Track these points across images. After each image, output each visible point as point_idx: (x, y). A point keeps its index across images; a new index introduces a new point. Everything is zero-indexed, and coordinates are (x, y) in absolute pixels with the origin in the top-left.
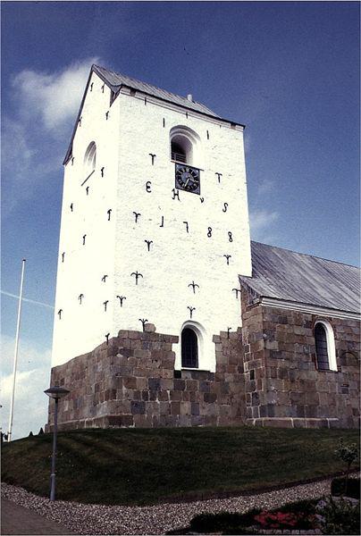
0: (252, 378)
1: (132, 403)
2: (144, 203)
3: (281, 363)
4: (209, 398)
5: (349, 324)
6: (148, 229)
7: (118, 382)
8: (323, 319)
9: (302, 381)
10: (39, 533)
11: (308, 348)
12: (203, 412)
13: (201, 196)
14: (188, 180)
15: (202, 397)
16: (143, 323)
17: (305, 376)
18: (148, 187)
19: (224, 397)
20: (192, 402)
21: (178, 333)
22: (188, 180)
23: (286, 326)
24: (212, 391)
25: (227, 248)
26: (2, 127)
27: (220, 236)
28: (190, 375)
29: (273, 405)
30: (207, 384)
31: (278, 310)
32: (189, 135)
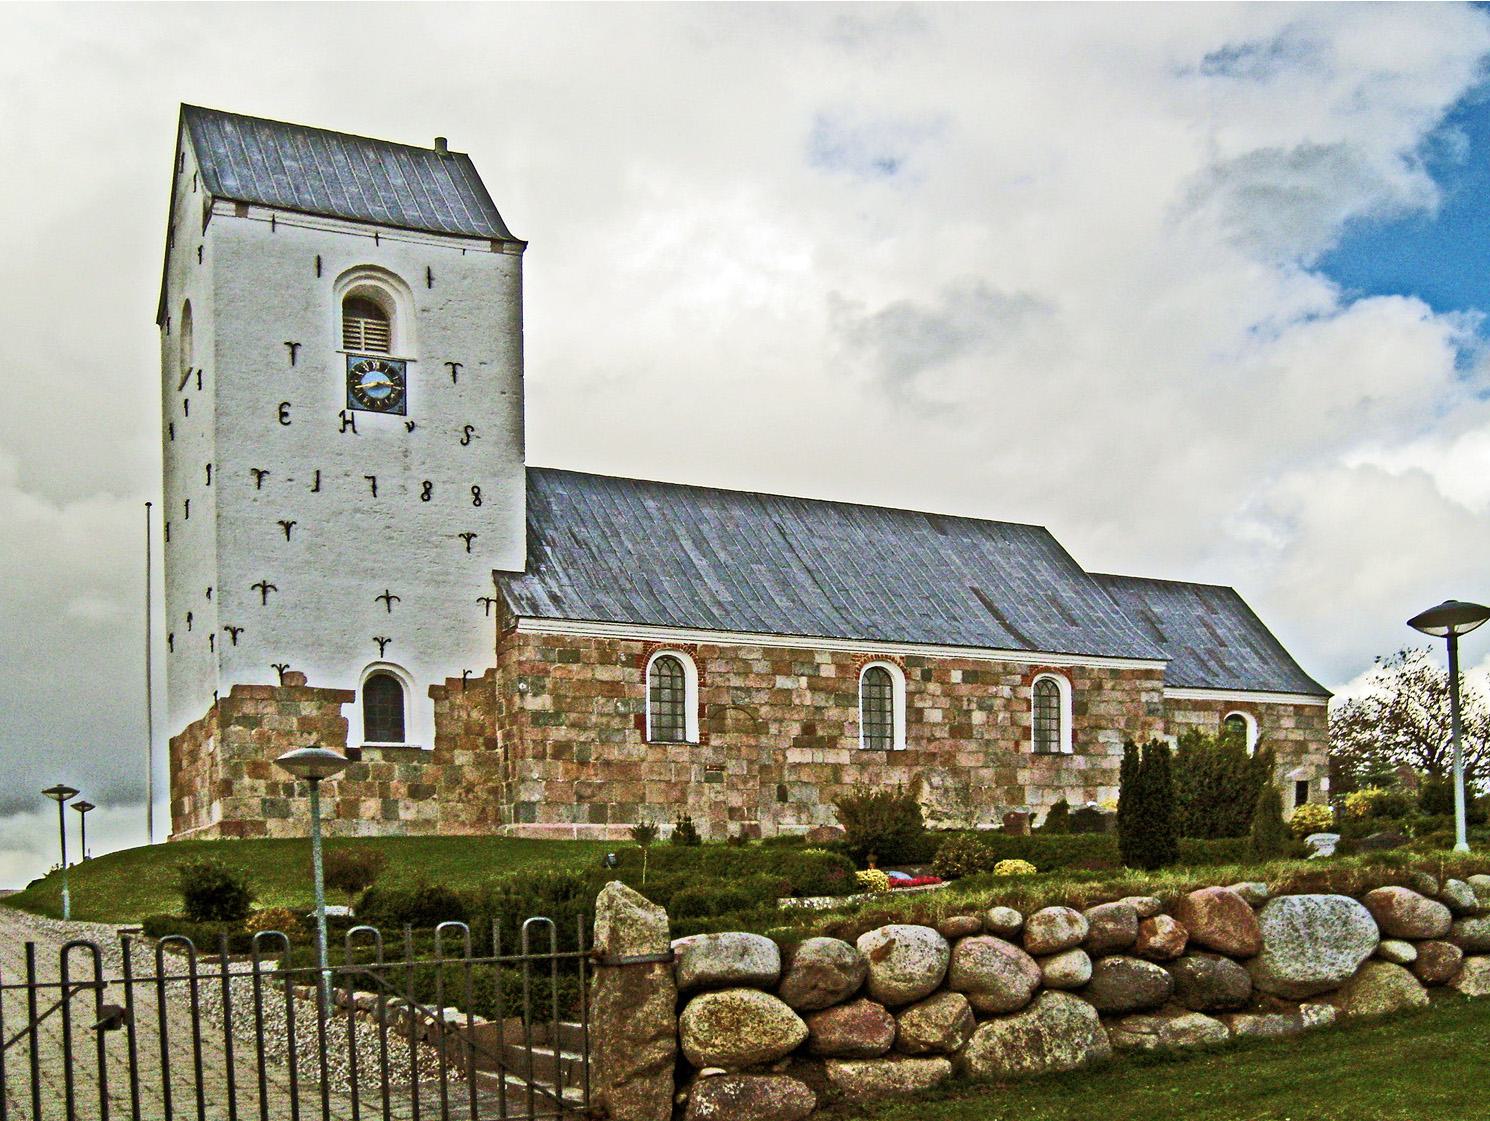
0: (506, 759)
1: (264, 801)
2: (277, 449)
3: (559, 733)
4: (417, 792)
5: (742, 654)
6: (284, 497)
7: (236, 771)
8: (676, 647)
9: (607, 764)
10: (680, 719)
11: (626, 704)
12: (405, 815)
13: (408, 419)
14: (379, 390)
15: (403, 790)
16: (281, 670)
17: (614, 754)
18: (283, 415)
19: (449, 789)
20: (384, 795)
21: (356, 683)
22: (379, 390)
23: (575, 667)
24: (426, 781)
25: (472, 518)
26: (219, 117)
27: (452, 498)
28: (378, 756)
29: (534, 804)
30: (415, 769)
31: (559, 640)
32: (386, 281)
